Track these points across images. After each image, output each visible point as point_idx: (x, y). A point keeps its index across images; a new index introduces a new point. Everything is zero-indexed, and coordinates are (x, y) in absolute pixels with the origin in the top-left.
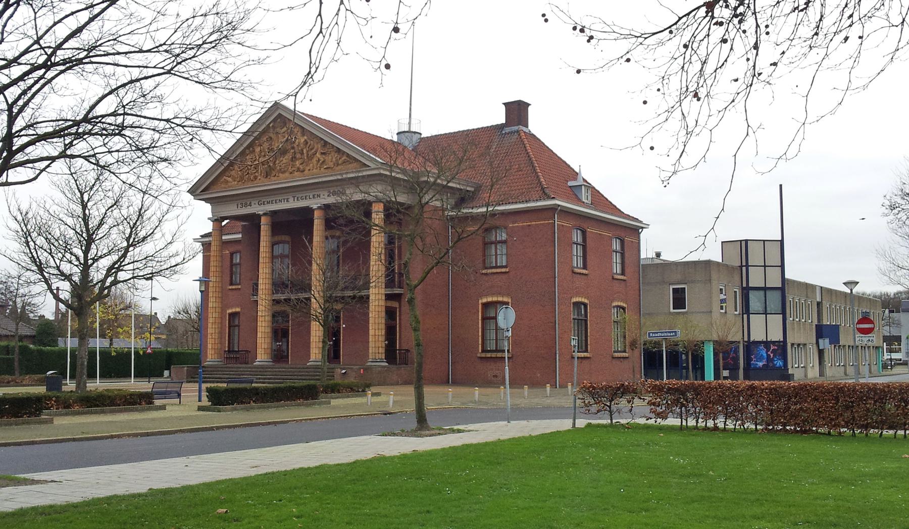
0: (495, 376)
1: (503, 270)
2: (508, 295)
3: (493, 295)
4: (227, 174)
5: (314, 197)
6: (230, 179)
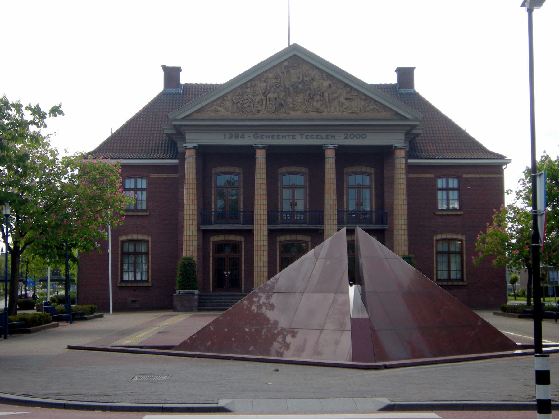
1: (144, 214)
2: (462, 233)
3: (447, 232)
4: (219, 102)
5: (327, 137)
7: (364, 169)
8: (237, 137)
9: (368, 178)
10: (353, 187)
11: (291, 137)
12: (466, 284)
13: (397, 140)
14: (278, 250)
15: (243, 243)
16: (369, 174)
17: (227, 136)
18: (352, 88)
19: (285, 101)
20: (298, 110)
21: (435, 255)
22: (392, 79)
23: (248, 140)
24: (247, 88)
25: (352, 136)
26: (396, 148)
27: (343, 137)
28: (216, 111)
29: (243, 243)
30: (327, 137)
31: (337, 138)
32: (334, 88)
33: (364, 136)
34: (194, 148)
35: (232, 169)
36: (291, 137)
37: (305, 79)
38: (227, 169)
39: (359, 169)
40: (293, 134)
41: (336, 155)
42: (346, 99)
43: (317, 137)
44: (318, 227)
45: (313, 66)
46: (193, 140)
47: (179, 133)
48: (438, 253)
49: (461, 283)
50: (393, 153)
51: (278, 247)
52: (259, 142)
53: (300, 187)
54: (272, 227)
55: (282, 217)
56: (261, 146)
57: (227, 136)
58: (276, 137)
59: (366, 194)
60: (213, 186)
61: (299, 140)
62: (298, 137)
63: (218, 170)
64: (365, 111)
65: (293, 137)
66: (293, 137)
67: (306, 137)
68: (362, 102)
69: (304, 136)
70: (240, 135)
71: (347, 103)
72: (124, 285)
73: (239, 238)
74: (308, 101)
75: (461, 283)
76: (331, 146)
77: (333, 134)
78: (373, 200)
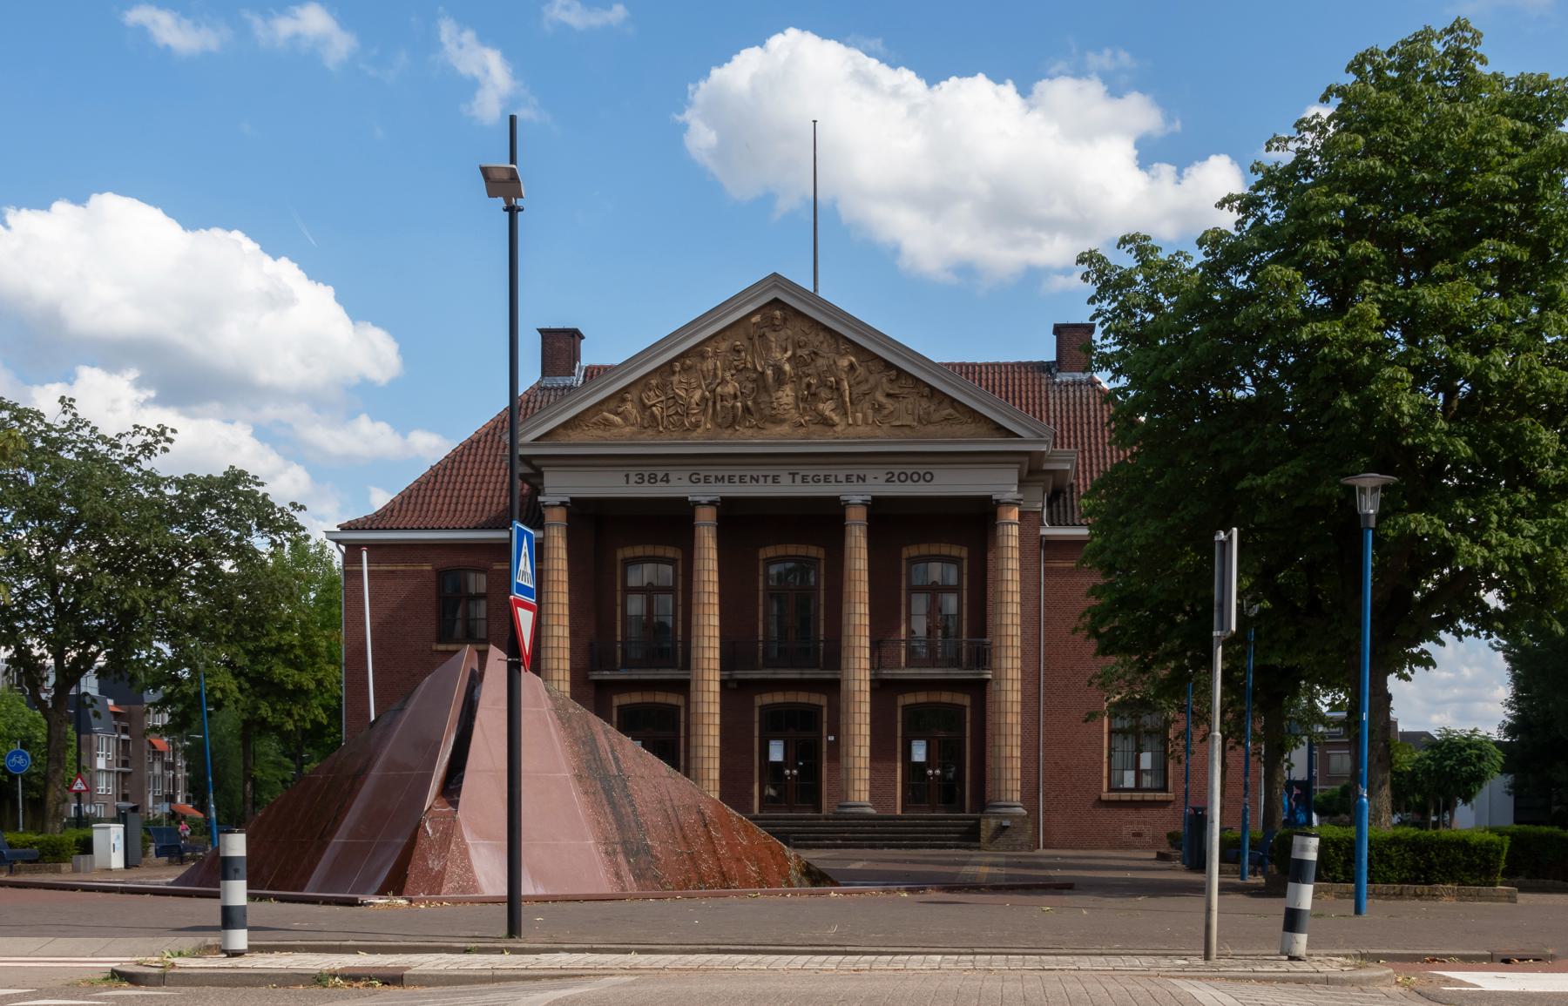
0: (1138, 835)
4: (612, 405)
5: (848, 479)
6: (617, 419)
7: (945, 550)
8: (653, 479)
9: (669, 569)
10: (637, 590)
11: (770, 480)
12: (1170, 796)
13: (1001, 484)
14: (757, 725)
15: (968, 711)
16: (671, 561)
17: (633, 478)
18: (900, 371)
19: (755, 401)
20: (782, 421)
21: (1106, 737)
22: (1046, 351)
23: (678, 486)
24: (674, 373)
25: (903, 477)
26: (698, 503)
27: (883, 477)
28: (608, 424)
29: (825, 711)
30: (848, 479)
31: (869, 480)
32: (861, 370)
33: (928, 477)
34: (563, 504)
35: (660, 551)
36: (770, 480)
37: (799, 352)
38: (649, 550)
39: (934, 549)
40: (772, 473)
41: (870, 517)
42: (888, 395)
43: (816, 480)
44: (827, 675)
45: (818, 323)
46: (559, 488)
47: (533, 471)
48: (1111, 732)
49: (1160, 796)
50: (692, 518)
51: (757, 718)
52: (703, 491)
53: (949, 589)
54: (740, 675)
55: (624, 651)
56: (704, 500)
57: (633, 478)
58: (736, 479)
59: (951, 603)
60: (761, 586)
61: (787, 487)
62: (785, 479)
63: (628, 552)
64: (930, 423)
65: (775, 480)
66: (775, 480)
67: (804, 479)
68: (925, 403)
69: (798, 478)
70: (660, 475)
71: (890, 405)
72: (1114, 796)
73: (965, 700)
74: (804, 400)
75: (1160, 796)
76: (857, 499)
77: (861, 474)
78: (965, 616)
